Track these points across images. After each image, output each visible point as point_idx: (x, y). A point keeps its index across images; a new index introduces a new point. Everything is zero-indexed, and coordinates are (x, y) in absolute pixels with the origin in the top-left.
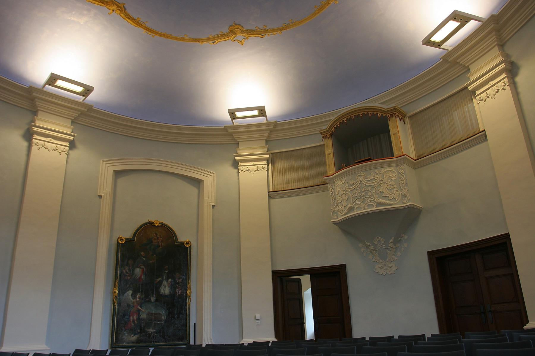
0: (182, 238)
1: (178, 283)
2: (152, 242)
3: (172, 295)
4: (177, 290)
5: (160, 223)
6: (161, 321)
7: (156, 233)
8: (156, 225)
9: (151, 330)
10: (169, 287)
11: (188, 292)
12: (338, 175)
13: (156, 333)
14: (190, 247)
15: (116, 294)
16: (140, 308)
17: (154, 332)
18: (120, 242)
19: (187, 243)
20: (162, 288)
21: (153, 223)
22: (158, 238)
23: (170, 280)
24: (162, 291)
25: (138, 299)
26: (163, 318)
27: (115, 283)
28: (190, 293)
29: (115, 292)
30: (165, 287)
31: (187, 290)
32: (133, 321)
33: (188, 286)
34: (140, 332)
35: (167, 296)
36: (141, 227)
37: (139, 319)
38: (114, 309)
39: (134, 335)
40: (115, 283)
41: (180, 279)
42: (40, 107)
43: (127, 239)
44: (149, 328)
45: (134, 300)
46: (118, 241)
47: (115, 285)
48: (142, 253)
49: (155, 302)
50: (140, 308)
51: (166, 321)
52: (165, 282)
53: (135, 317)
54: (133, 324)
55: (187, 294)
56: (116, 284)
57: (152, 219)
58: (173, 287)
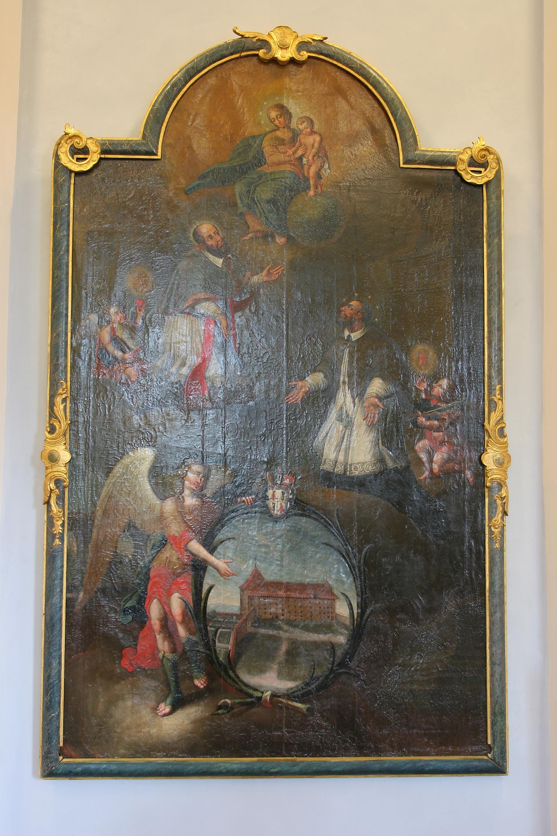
0: (443, 130)
1: (423, 406)
2: (260, 160)
3: (394, 481)
4: (422, 445)
5: (302, 46)
6: (328, 628)
7: (281, 107)
8: (282, 55)
9: (270, 682)
10: (371, 426)
11: (488, 459)
12: (490, 563)
13: (303, 697)
14: (495, 183)
15: (61, 471)
16: (203, 553)
17: (290, 695)
18: (67, 161)
19: (477, 164)
20: (331, 427)
21: (264, 44)
22: (295, 136)
23: (377, 386)
24: (330, 453)
25: (190, 501)
26: (342, 610)
27: (52, 405)
28: (503, 463)
29: (53, 459)
30: (349, 425)
31: (480, 447)
32: (166, 619)
33: (490, 425)
34: (210, 691)
35: (361, 483)
36: (191, 71)
37: (198, 610)
38: (52, 557)
39: (176, 706)
40: (52, 405)
41: (435, 378)
42: (271, 769)
43: (109, 149)
44: (262, 670)
45: (169, 505)
46: (57, 157)
47: (52, 414)
48: (206, 228)
49: (287, 515)
50: (203, 553)
51: (358, 631)
52: (345, 398)
53: (176, 604)
54: (163, 645)
55: (481, 471)
56: (59, 408)
57: (254, 27)
58: (393, 430)
